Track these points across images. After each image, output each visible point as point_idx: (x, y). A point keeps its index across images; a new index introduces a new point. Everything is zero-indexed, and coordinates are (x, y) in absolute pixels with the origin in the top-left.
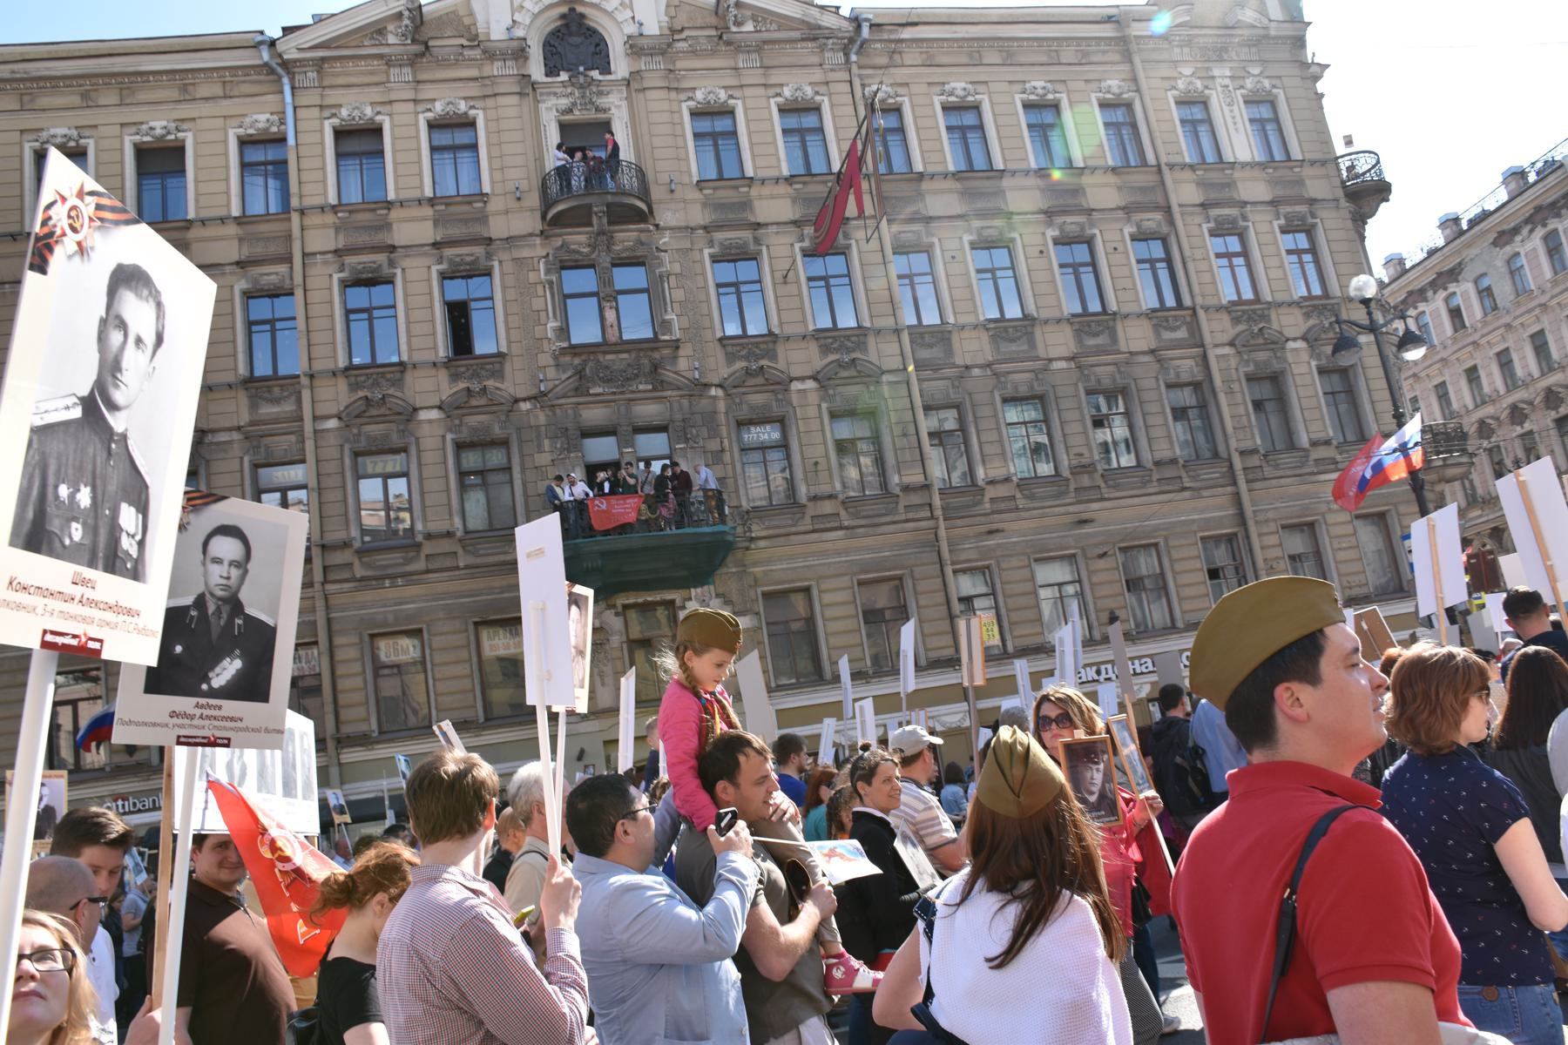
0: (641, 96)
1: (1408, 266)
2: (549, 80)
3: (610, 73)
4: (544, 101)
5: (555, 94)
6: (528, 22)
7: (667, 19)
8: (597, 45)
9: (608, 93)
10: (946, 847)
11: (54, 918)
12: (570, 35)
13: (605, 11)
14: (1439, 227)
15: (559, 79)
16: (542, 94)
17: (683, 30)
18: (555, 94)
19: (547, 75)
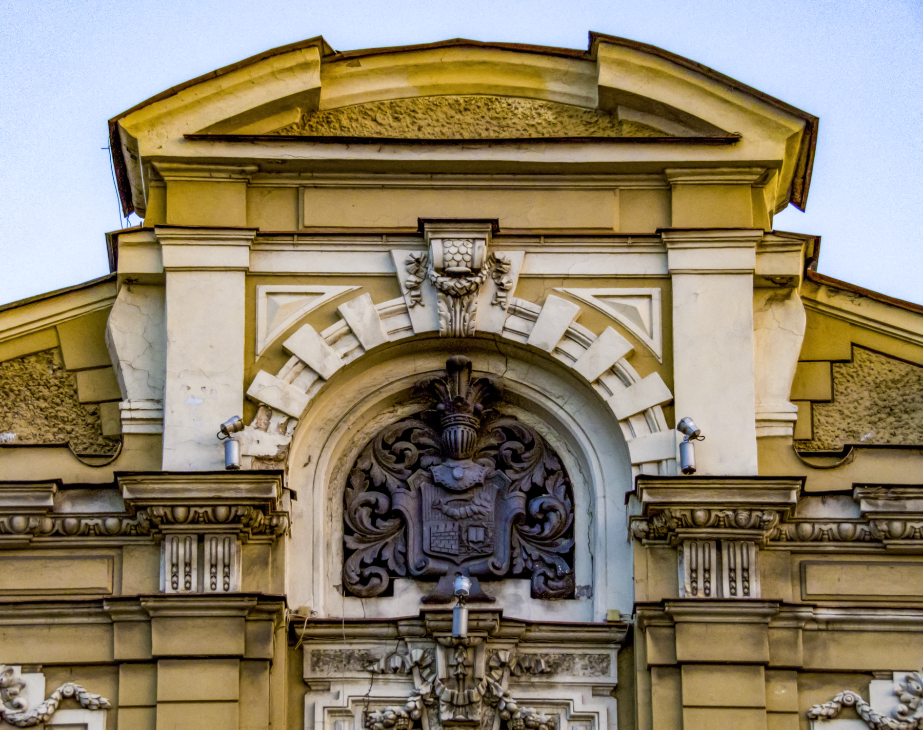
0: (662, 691)
1: (656, 346)
2: (354, 609)
3: (569, 594)
4: (324, 686)
5: (367, 660)
6: (331, 364)
7: (790, 411)
8: (535, 491)
9: (554, 667)
10: (608, 518)
11: (661, 132)
12: (448, 452)
13: (602, 410)
14: (184, 135)
15: (391, 608)
16: (318, 660)
17: (843, 455)
18: (367, 660)
19: (347, 590)
